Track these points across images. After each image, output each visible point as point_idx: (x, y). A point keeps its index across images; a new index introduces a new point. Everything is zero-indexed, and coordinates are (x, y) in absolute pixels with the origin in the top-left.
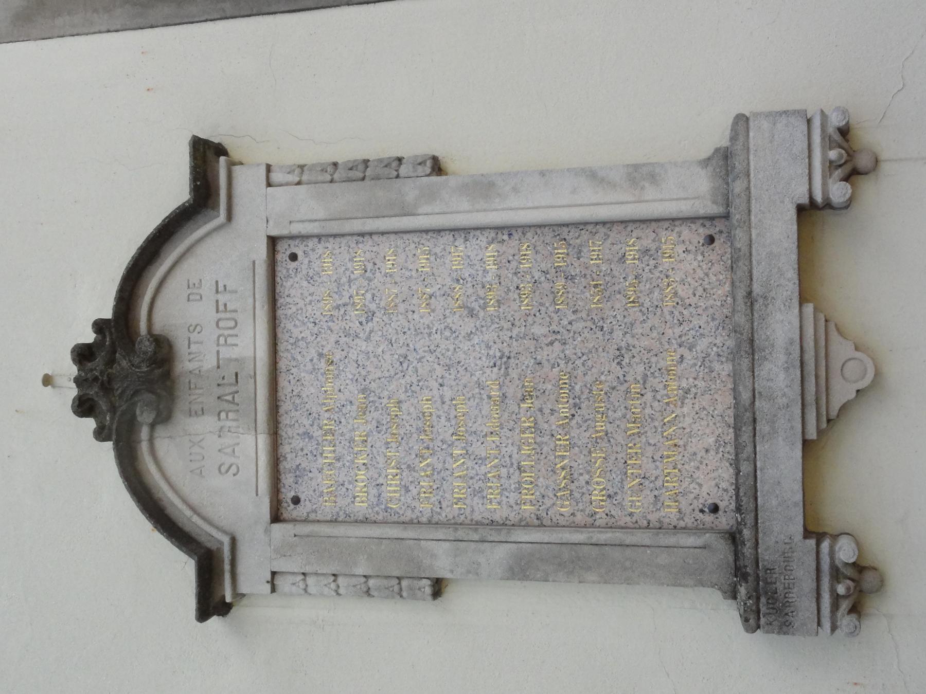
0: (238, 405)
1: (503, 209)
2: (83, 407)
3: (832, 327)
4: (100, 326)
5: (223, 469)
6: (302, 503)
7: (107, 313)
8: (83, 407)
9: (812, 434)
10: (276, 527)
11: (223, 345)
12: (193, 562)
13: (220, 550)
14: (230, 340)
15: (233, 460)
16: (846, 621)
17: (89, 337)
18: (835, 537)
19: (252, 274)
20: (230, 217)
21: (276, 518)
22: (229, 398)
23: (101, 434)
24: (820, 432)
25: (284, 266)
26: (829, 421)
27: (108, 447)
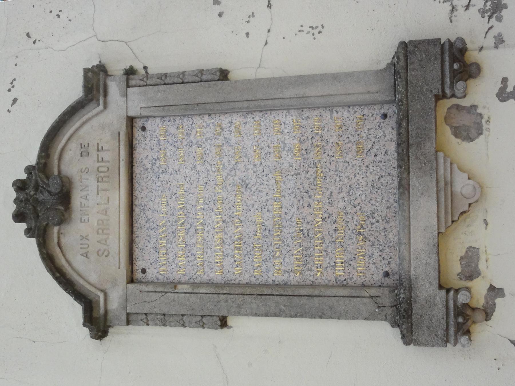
0: (108, 246)
1: (175, 293)
2: (19, 217)
3: (455, 166)
4: (29, 170)
5: (100, 253)
6: (147, 270)
7: (32, 159)
8: (19, 217)
9: (443, 230)
10: (130, 286)
11: (101, 182)
12: (81, 307)
13: (98, 302)
14: (105, 231)
15: (105, 247)
16: (464, 339)
17: (23, 176)
18: (457, 291)
19: (118, 144)
20: (105, 106)
21: (131, 280)
22: (104, 242)
23: (29, 232)
24: (447, 228)
25: (138, 134)
26: (453, 222)
27: (33, 241)
